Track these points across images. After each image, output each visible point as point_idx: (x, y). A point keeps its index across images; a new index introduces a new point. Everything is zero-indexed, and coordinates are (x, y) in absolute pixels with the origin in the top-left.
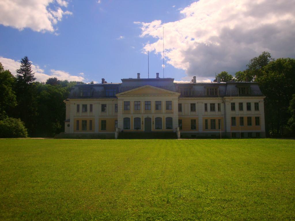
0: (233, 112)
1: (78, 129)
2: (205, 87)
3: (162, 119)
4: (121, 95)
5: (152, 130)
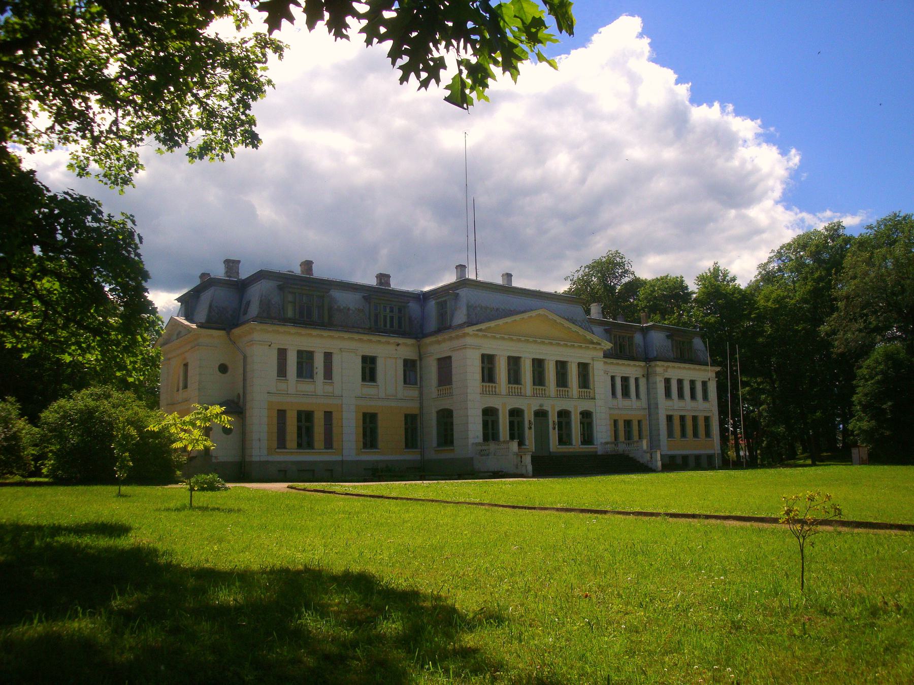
0: (369, 390)
1: (282, 442)
2: (281, 288)
3: (550, 412)
4: (477, 330)
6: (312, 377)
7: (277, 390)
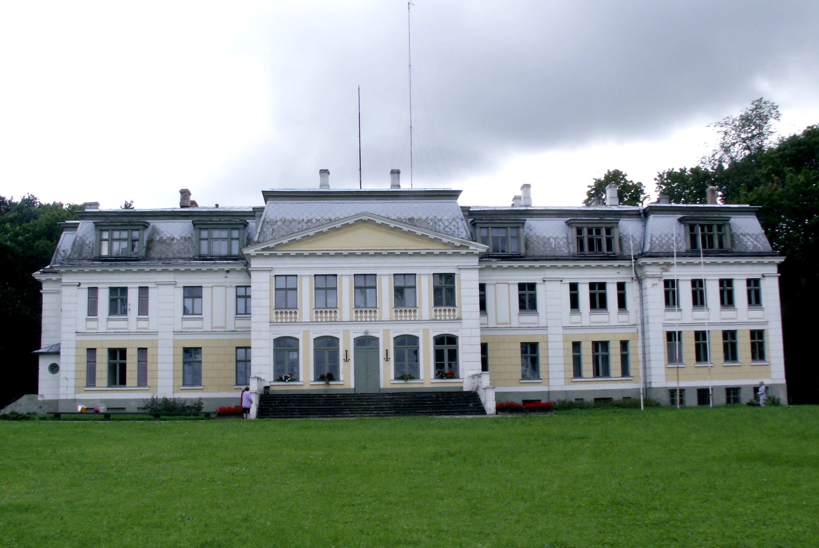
4: (263, 250)
5: (382, 386)
6: (125, 312)
7: (497, 324)
